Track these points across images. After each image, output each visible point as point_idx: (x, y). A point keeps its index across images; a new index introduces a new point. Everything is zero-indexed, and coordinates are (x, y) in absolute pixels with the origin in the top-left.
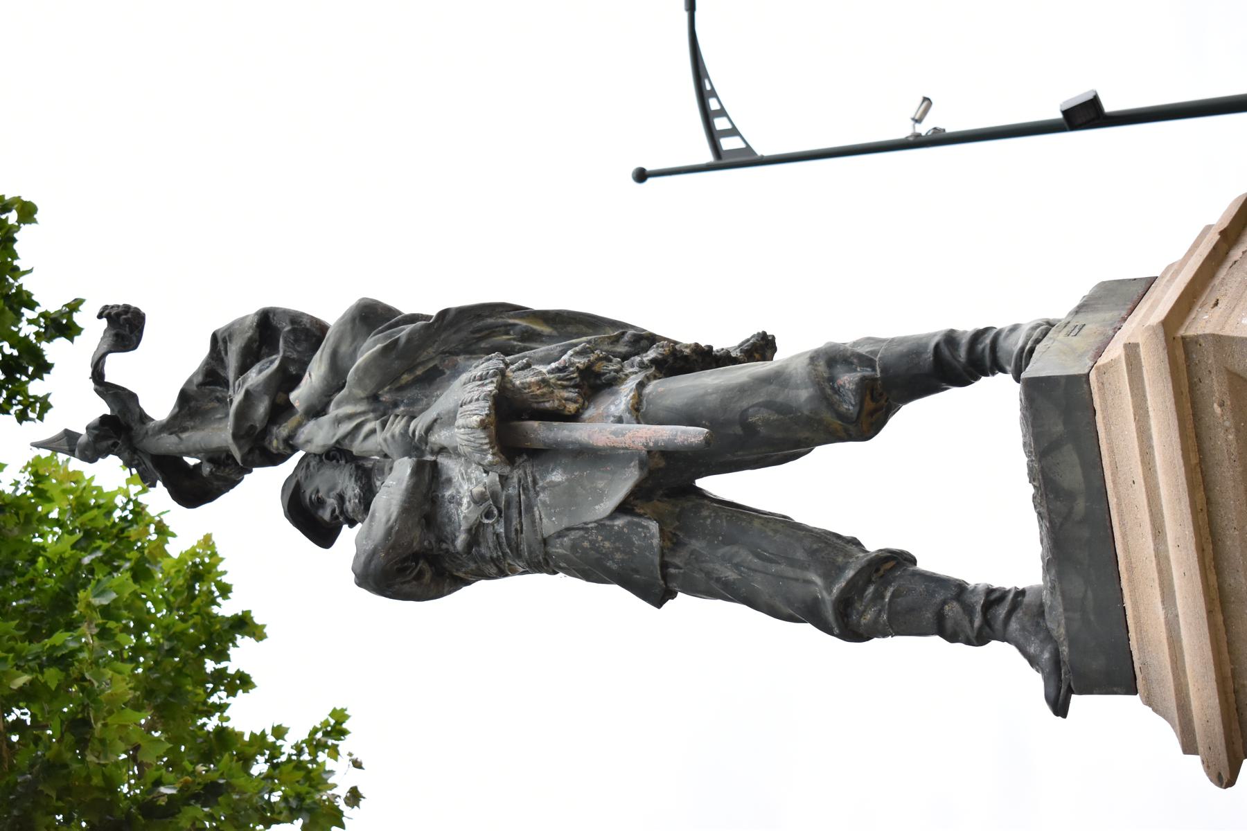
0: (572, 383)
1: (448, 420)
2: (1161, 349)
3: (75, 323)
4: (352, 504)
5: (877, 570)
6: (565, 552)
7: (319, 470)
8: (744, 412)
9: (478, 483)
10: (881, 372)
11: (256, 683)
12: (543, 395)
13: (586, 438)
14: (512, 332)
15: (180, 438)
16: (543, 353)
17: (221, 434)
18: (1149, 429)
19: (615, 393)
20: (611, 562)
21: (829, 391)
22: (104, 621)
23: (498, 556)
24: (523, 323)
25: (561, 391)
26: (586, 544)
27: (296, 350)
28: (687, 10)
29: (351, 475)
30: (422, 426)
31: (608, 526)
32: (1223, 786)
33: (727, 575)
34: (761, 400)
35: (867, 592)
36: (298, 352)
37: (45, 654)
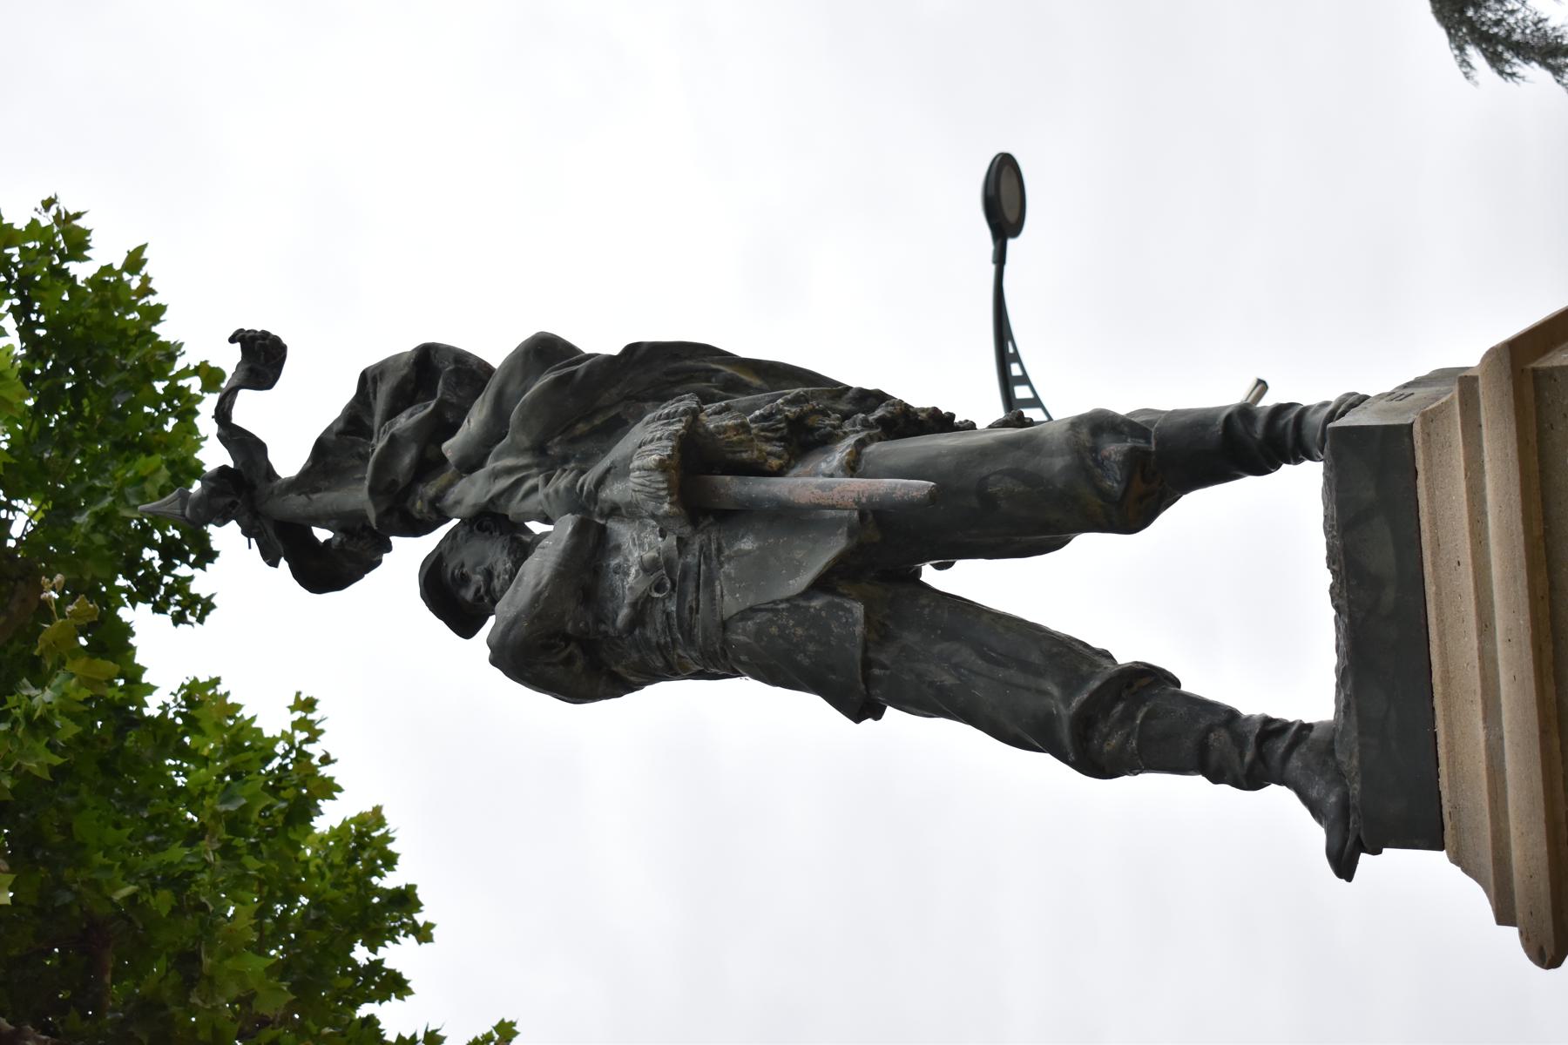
0: (778, 435)
1: (620, 471)
4: (501, 581)
5: (1130, 685)
6: (748, 640)
7: (466, 542)
8: (983, 480)
9: (651, 548)
10: (1157, 445)
12: (741, 442)
13: (786, 494)
14: (713, 380)
15: (309, 498)
17: (357, 496)
18: (1484, 489)
19: (832, 451)
20: (802, 655)
22: (230, 837)
23: (666, 643)
24: (728, 370)
25: (763, 443)
26: (774, 630)
27: (456, 394)
28: (995, 262)
30: (592, 479)
31: (803, 607)
32: (1546, 965)
33: (943, 678)
34: (1005, 467)
35: (1115, 711)
37: (161, 873)
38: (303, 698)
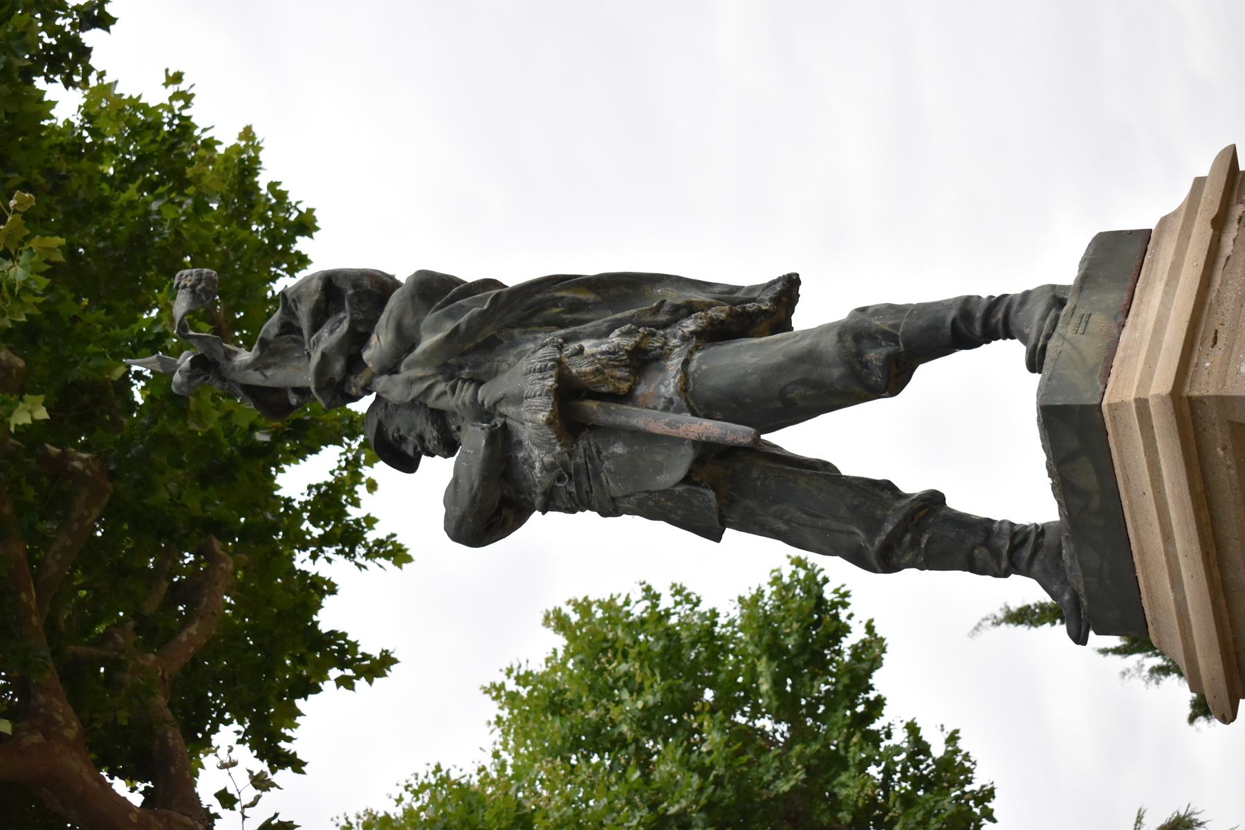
0: (623, 364)
2: (1169, 414)
3: (108, 14)
5: (913, 519)
8: (783, 391)
10: (904, 346)
11: (312, 260)
12: (599, 382)
14: (560, 304)
15: (265, 376)
16: (592, 329)
18: (1159, 462)
19: (663, 370)
21: (858, 367)
26: (651, 503)
29: (427, 419)
34: (797, 378)
35: (905, 540)
36: (363, 312)
38: (171, 74)
